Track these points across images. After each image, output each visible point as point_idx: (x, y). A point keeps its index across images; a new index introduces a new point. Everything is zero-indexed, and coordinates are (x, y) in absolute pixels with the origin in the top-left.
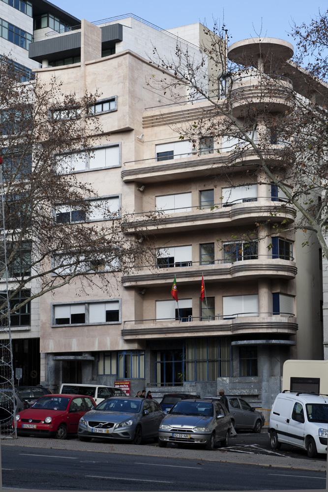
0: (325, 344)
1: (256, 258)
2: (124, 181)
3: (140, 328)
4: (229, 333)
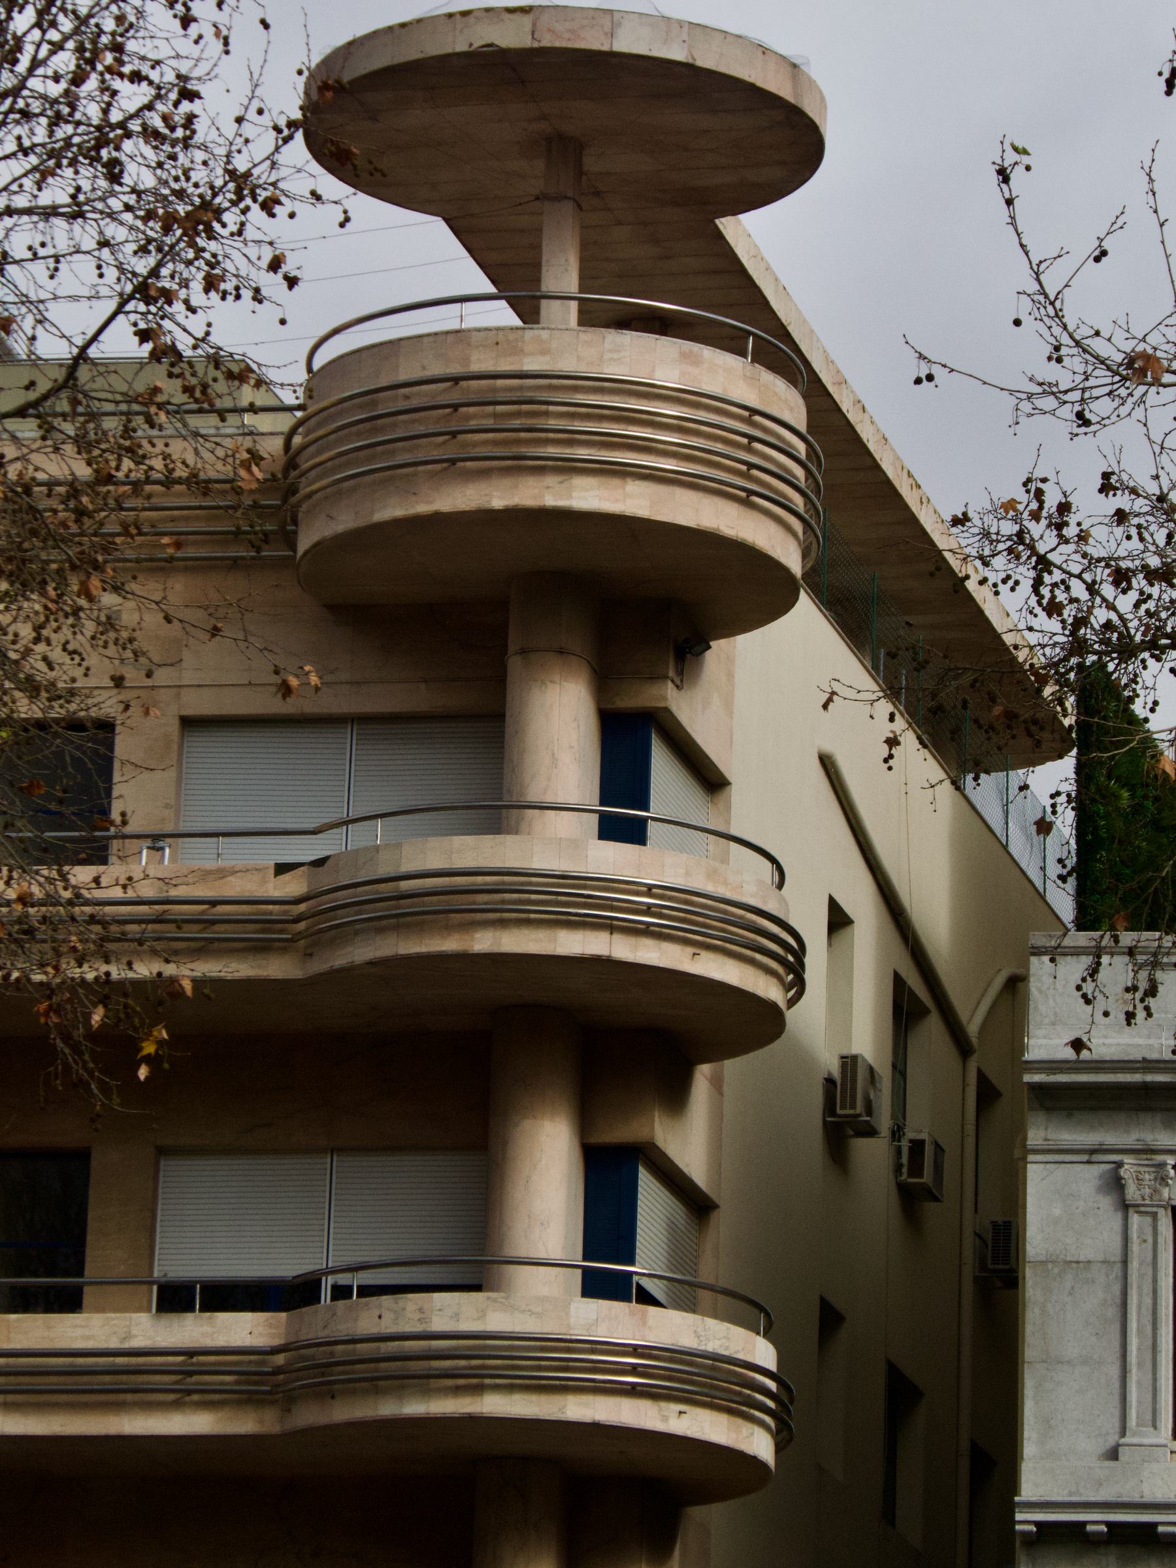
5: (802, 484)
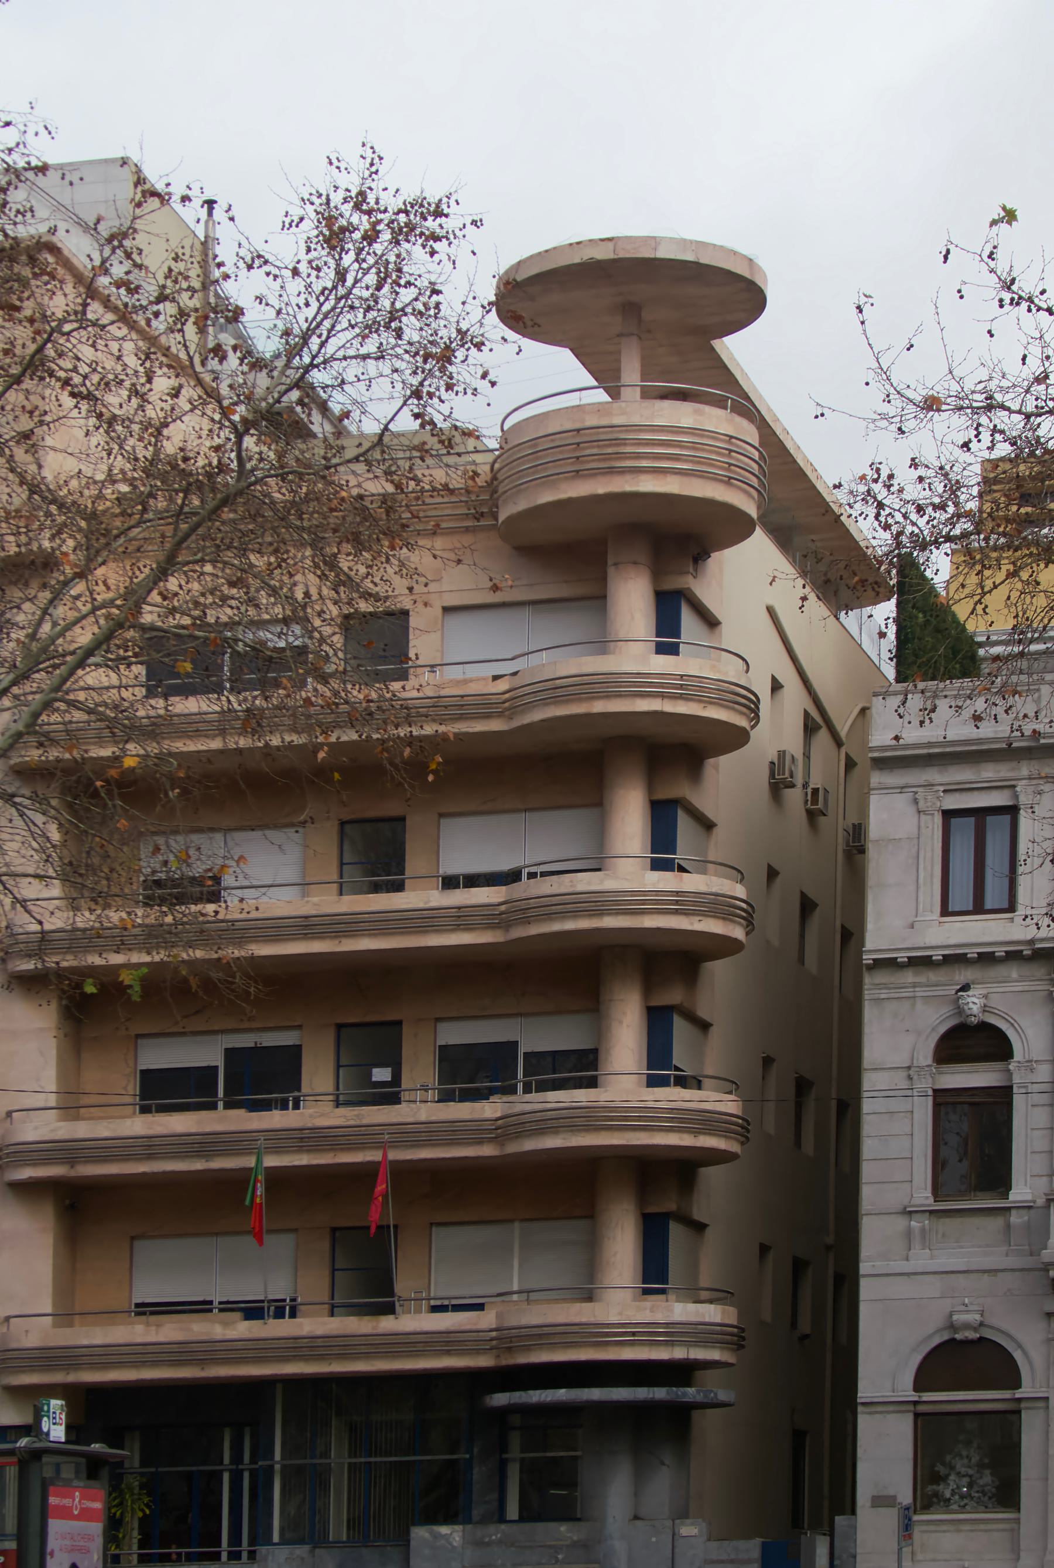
0: (863, 1404)
1: (592, 1083)
2: (11, 768)
3: (85, 1342)
4: (484, 1361)
5: (757, 459)
